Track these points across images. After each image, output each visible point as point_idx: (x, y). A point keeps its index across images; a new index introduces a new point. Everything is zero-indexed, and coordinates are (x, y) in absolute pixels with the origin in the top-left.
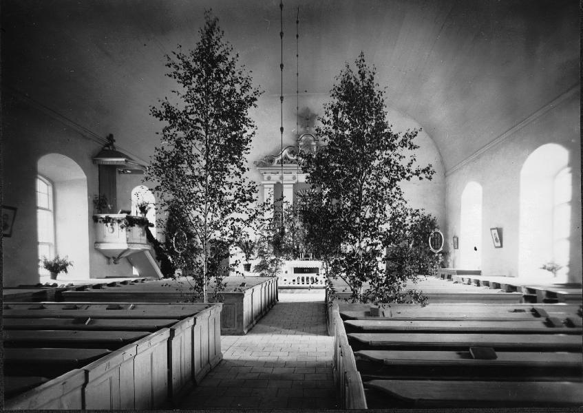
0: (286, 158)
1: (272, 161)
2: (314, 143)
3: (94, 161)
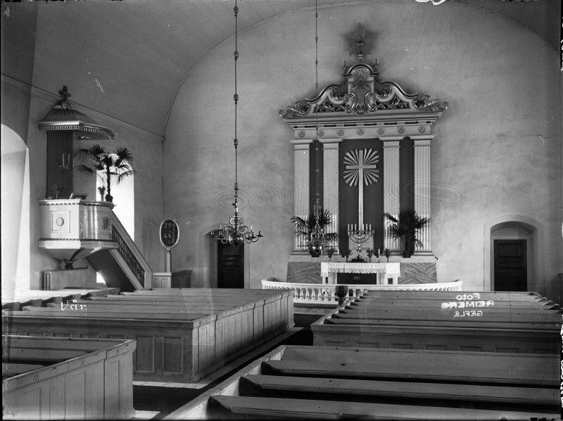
1: (305, 109)
2: (371, 79)
3: (40, 127)
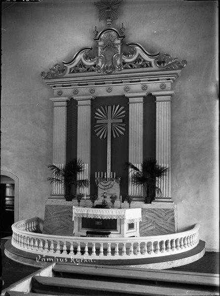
0: (81, 64)
2: (118, 41)
